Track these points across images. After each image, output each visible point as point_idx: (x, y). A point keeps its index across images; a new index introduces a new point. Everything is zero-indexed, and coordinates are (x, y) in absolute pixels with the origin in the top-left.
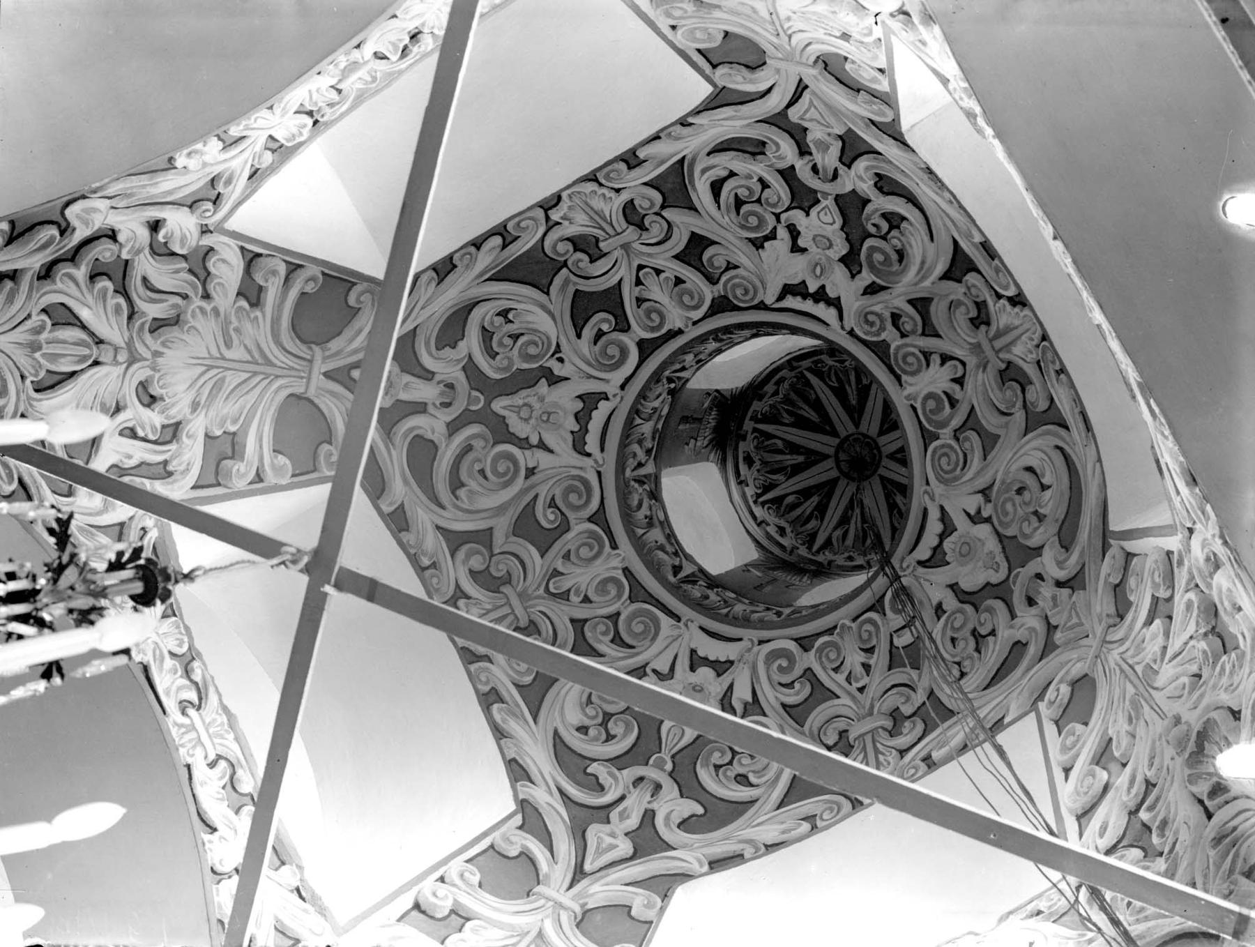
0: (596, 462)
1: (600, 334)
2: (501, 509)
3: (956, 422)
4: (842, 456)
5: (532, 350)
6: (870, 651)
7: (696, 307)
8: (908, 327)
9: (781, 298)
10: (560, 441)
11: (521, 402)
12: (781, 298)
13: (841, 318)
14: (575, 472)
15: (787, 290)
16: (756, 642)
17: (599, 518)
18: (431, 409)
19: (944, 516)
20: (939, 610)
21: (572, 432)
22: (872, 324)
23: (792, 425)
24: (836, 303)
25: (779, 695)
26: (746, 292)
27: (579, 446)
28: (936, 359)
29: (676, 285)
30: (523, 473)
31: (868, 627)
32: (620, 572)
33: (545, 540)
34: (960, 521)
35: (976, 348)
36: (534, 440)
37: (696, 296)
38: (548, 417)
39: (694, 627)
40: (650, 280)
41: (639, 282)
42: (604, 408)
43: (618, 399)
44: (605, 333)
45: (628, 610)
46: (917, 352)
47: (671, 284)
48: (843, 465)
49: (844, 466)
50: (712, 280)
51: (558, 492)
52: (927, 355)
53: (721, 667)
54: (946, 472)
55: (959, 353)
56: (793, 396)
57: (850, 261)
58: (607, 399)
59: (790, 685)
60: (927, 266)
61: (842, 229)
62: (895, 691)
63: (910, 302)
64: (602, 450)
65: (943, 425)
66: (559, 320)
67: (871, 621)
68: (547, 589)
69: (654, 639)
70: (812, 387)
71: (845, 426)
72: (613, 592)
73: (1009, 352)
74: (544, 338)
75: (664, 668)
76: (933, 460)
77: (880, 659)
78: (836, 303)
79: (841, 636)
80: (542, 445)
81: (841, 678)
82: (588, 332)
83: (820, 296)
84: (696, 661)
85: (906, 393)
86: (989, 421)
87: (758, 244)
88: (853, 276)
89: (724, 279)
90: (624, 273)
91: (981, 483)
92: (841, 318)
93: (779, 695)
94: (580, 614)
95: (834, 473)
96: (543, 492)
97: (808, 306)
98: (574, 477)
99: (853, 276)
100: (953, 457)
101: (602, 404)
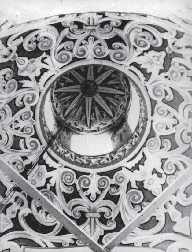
0: (127, 67)
1: (167, 94)
2: (128, 36)
3: (78, 188)
4: (92, 84)
5: (174, 74)
6: (22, 131)
7: (156, 126)
8: (112, 190)
9: (143, 154)
10: (140, 60)
11: (160, 59)
12: (143, 154)
13: (127, 168)
14: (127, 59)
15: (144, 158)
16: (41, 91)
17: (108, 58)
18: (175, 39)
19: (52, 169)
20: (24, 158)
21: (141, 65)
22: (120, 178)
23: (110, 75)
24: (132, 170)
25: (20, 97)
26: (151, 146)
27: (134, 64)
28: (99, 192)
29: (167, 126)
30: (136, 46)
31: (30, 131)
32: (86, 57)
33: (110, 42)
34: (48, 174)
35: (94, 211)
36: (145, 54)
37: (159, 129)
38: (150, 63)
39: (55, 73)
40: (173, 121)
41: (174, 117)
42: (143, 78)
43: (143, 84)
44: (166, 95)
45: (71, 55)
46: (104, 187)
47: (168, 127)
48: (89, 83)
49: (89, 83)
50: (162, 137)
51: (123, 52)
52: (102, 190)
53: (38, 79)
54: (65, 176)
55: (96, 203)
56: (118, 83)
57: (140, 185)
58: (145, 81)
59: (22, 100)
60: (125, 212)
61: (151, 191)
62: (7, 139)
63: (119, 195)
64: (130, 70)
65: (79, 182)
66: (179, 88)
67: (31, 132)
68: (91, 36)
69: (57, 60)
70: (118, 89)
71: (102, 89)
72: (80, 53)
73: (88, 224)
74: (176, 80)
75: (45, 61)
76: (72, 173)
77: (19, 133)
78: (132, 170)
79: (31, 121)
80: (142, 54)
81: (18, 119)
82: (170, 92)
83: (136, 167)
84: (43, 71)
85: (94, 175)
86: (73, 202)
87: (163, 161)
88: (136, 181)
89: (160, 142)
90: (179, 116)
91: (57, 189)
92: (127, 168)
93: (20, 97)
94: (77, 43)
95: (88, 78)
96: (126, 48)
97: (136, 161)
98: (125, 58)
99: (136, 181)
100: (68, 181)
101: (144, 79)
